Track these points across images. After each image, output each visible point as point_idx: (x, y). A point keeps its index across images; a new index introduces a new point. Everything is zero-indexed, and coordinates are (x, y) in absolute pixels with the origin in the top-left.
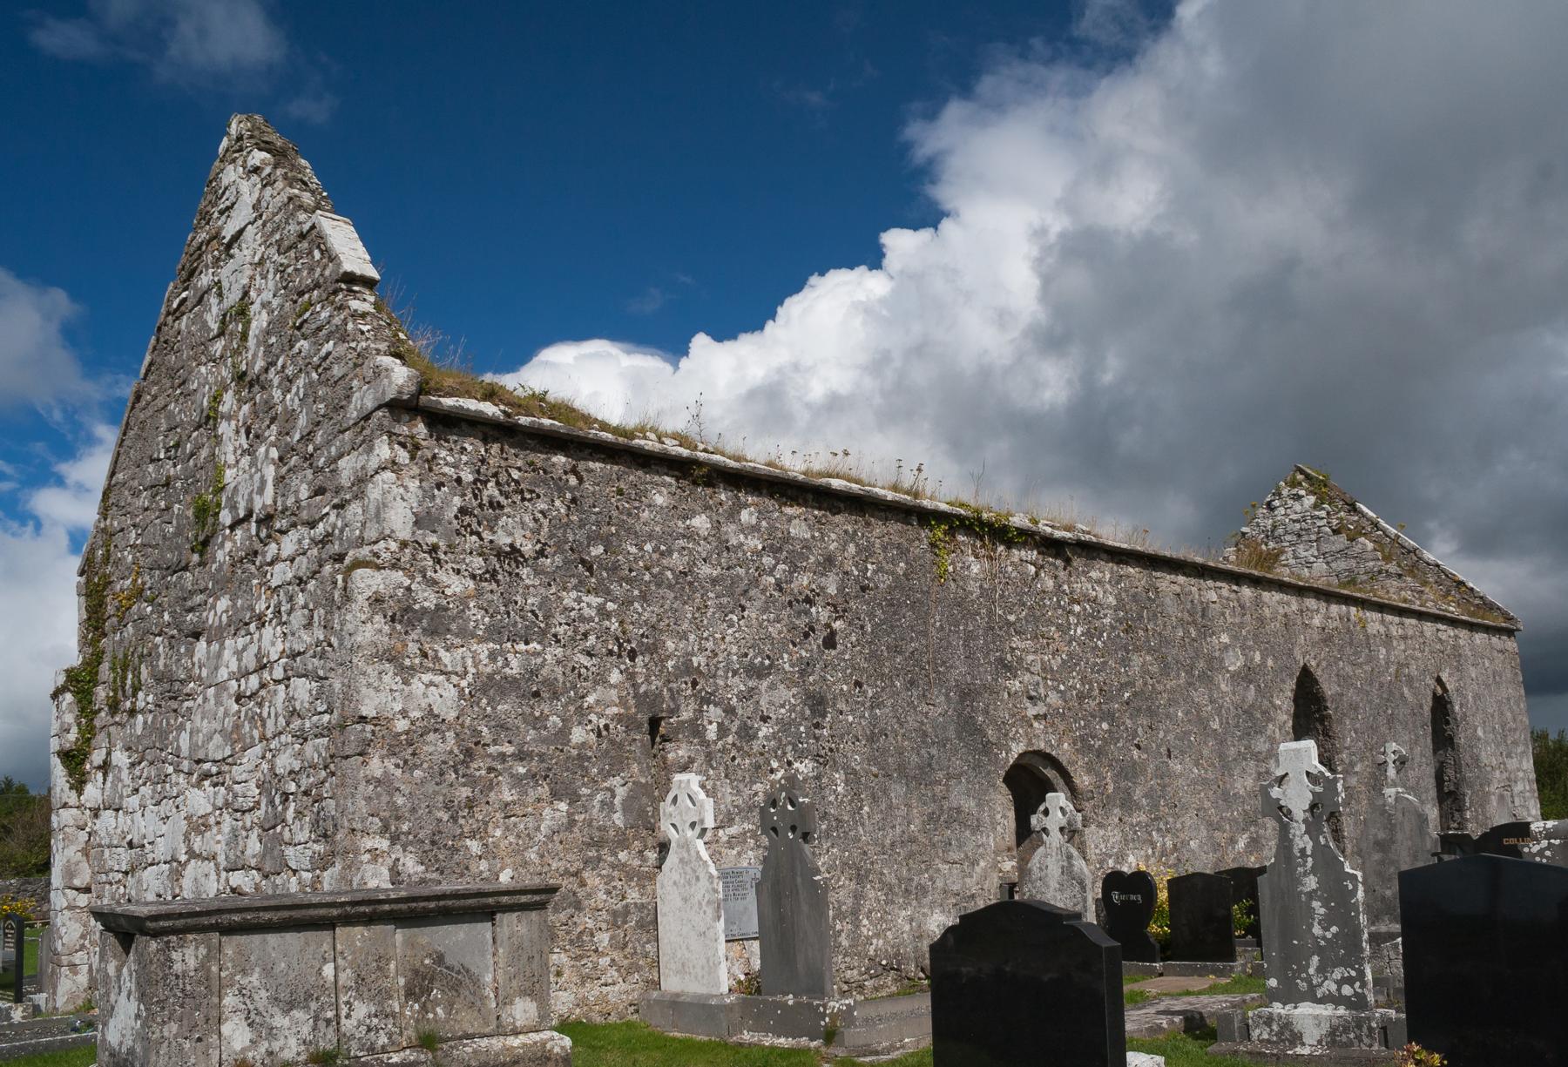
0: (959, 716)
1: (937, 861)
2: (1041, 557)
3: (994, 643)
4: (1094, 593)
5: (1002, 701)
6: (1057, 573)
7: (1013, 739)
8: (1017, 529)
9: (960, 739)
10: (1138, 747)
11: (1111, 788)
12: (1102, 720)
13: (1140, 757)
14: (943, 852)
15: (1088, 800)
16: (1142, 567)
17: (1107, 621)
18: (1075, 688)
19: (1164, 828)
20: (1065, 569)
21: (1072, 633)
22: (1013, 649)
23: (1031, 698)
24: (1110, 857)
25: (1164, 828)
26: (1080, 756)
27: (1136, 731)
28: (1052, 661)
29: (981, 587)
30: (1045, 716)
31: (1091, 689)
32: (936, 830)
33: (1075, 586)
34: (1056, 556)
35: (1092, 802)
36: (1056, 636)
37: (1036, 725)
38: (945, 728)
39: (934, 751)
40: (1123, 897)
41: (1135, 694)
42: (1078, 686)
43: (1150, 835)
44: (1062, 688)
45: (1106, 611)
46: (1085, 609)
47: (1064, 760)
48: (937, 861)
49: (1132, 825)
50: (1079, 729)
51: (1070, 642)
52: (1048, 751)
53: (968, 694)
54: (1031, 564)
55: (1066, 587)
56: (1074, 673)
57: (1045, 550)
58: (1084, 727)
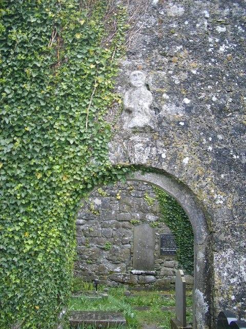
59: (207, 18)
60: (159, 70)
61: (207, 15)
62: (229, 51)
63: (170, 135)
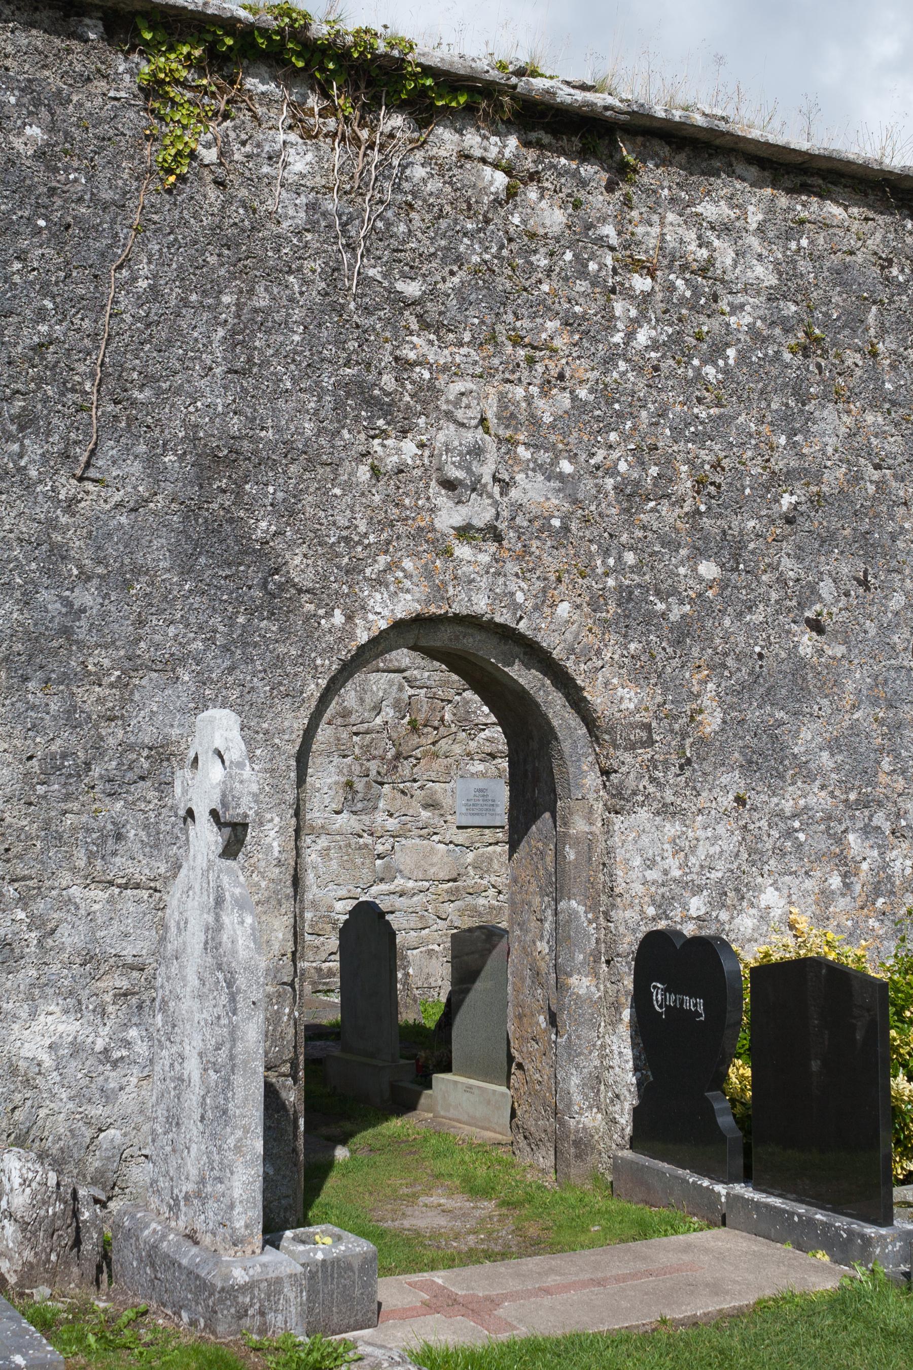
0: (190, 513)
1: (65, 878)
2: (532, 154)
3: (340, 344)
4: (704, 253)
5: (348, 486)
6: (582, 195)
7: (379, 582)
8: (428, 70)
9: (186, 571)
10: (816, 626)
11: (712, 722)
12: (699, 553)
13: (820, 652)
14: (91, 856)
15: (631, 747)
16: (870, 207)
17: (741, 321)
18: (612, 471)
19: (887, 827)
20: (610, 187)
21: (618, 338)
22: (403, 365)
23: (449, 485)
24: (698, 890)
25: (887, 827)
26: (613, 638)
27: (813, 588)
28: (540, 403)
29: (312, 207)
30: (494, 534)
31: (666, 478)
32: (67, 797)
33: (640, 230)
34: (584, 155)
35: (645, 754)
36: (558, 343)
37: (463, 551)
38: (131, 542)
39: (86, 597)
40: (671, 999)
41: (817, 501)
42: (623, 467)
43: (839, 840)
44: (566, 467)
45: (740, 299)
46: (672, 288)
47: (549, 640)
48: (65, 878)
49: (780, 815)
50: (620, 569)
51: (609, 361)
52: (503, 617)
53: (231, 463)
54: (496, 166)
55: (608, 230)
56: (613, 437)
57: (546, 139)
58: (637, 569)
59: (612, 249)
60: (508, 381)
61: (614, 241)
62: (655, 345)
63: (533, 549)
